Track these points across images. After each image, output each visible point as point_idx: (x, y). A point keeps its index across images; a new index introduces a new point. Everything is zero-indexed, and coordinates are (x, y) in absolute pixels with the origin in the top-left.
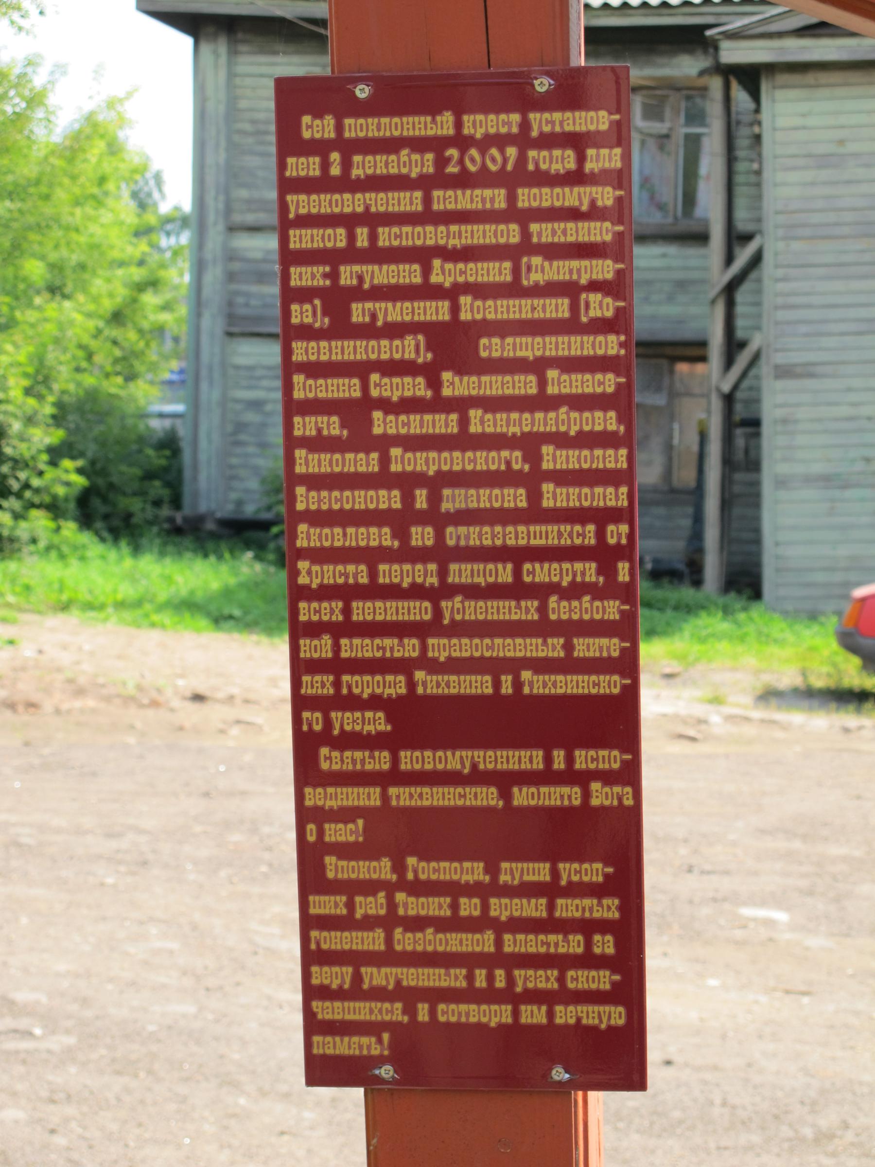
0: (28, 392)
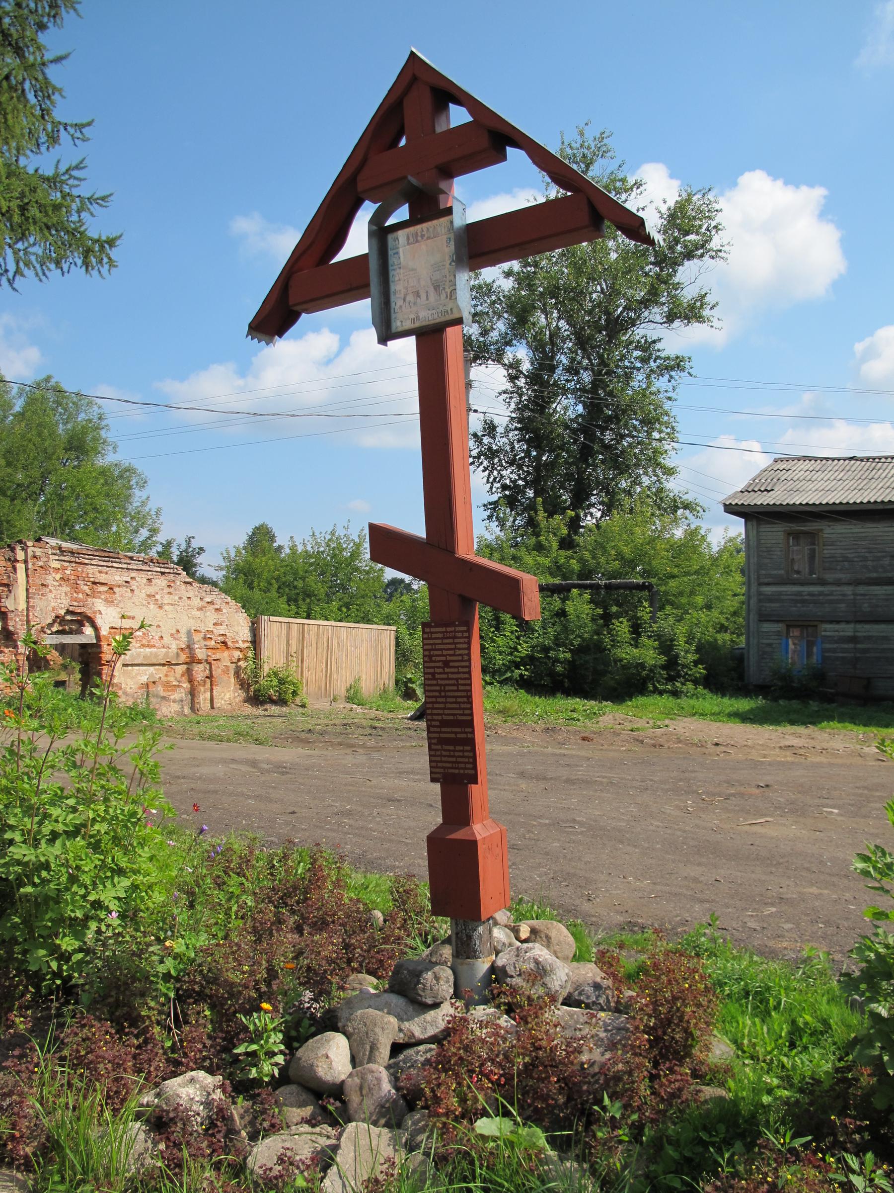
0: (686, 642)
